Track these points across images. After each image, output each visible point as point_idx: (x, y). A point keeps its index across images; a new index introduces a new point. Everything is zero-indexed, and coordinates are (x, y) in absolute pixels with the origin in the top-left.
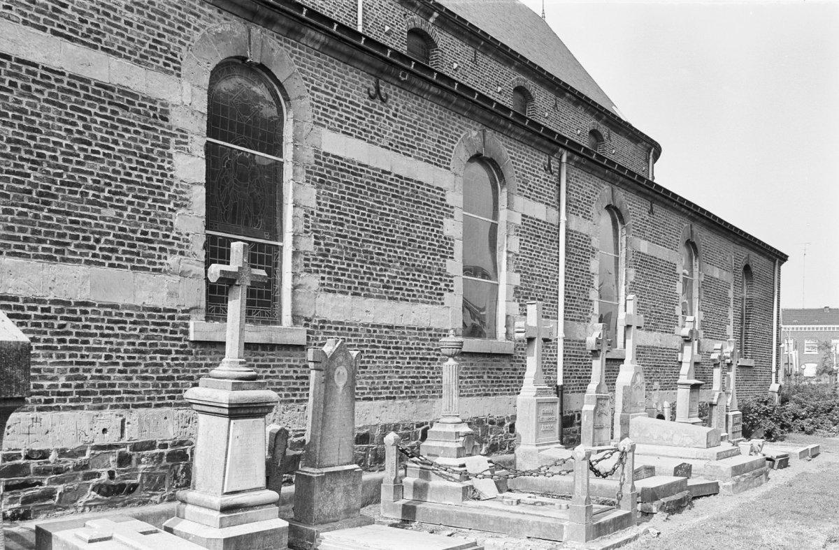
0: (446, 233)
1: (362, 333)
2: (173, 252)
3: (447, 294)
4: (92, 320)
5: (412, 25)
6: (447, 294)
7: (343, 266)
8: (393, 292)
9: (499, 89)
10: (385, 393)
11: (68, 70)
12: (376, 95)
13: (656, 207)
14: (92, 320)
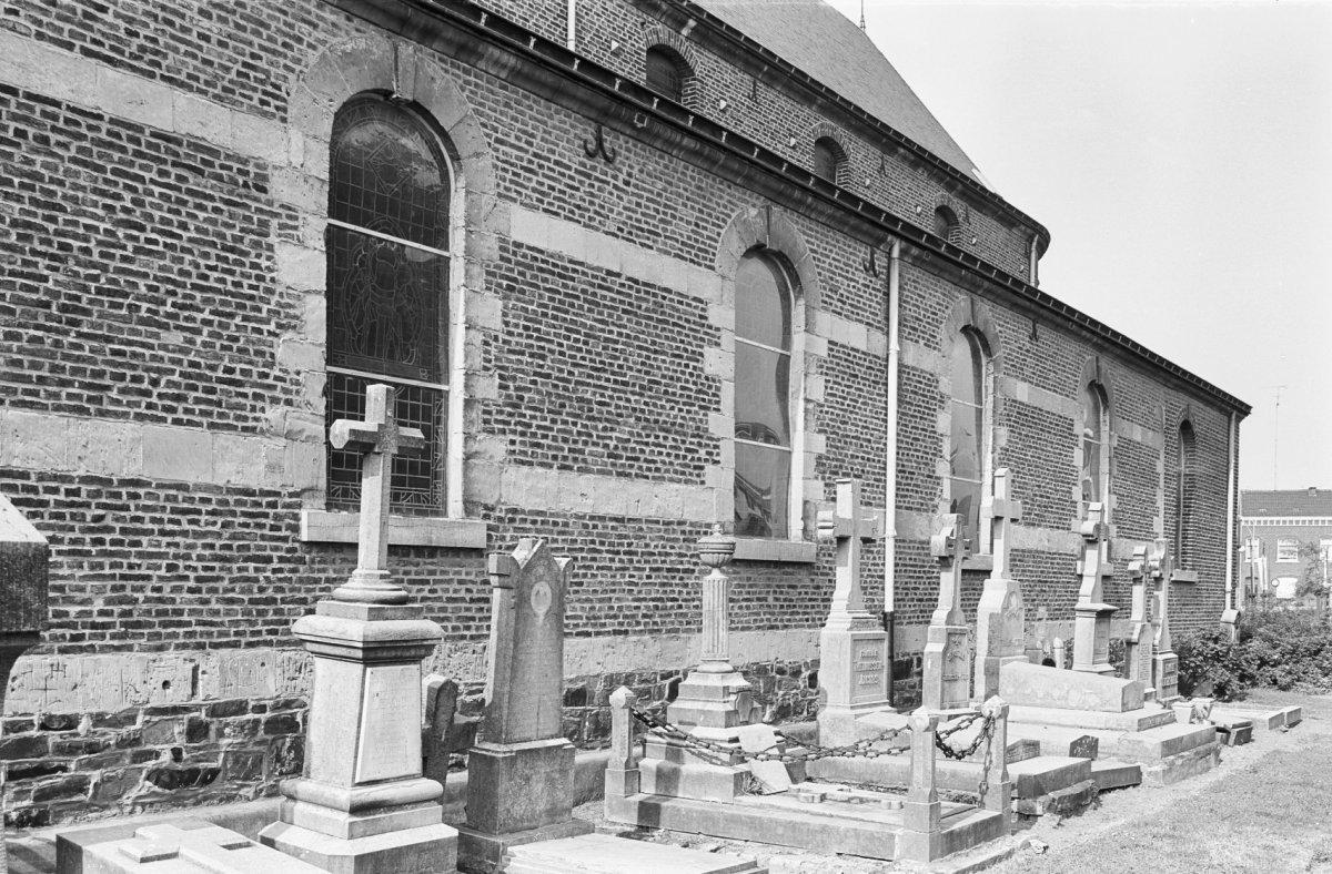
0: (709, 370)
1: (575, 529)
2: (275, 401)
3: (709, 468)
4: (146, 508)
5: (654, 41)
6: (709, 468)
7: (544, 423)
8: (624, 464)
9: (793, 141)
10: (611, 625)
11: (109, 111)
12: (597, 151)
13: (1041, 329)
14: (146, 508)
